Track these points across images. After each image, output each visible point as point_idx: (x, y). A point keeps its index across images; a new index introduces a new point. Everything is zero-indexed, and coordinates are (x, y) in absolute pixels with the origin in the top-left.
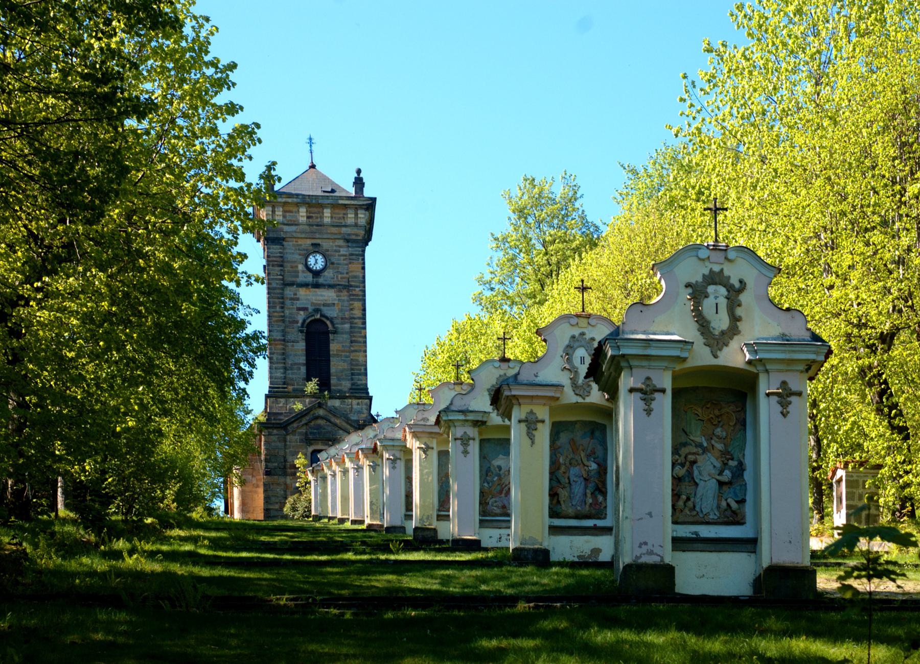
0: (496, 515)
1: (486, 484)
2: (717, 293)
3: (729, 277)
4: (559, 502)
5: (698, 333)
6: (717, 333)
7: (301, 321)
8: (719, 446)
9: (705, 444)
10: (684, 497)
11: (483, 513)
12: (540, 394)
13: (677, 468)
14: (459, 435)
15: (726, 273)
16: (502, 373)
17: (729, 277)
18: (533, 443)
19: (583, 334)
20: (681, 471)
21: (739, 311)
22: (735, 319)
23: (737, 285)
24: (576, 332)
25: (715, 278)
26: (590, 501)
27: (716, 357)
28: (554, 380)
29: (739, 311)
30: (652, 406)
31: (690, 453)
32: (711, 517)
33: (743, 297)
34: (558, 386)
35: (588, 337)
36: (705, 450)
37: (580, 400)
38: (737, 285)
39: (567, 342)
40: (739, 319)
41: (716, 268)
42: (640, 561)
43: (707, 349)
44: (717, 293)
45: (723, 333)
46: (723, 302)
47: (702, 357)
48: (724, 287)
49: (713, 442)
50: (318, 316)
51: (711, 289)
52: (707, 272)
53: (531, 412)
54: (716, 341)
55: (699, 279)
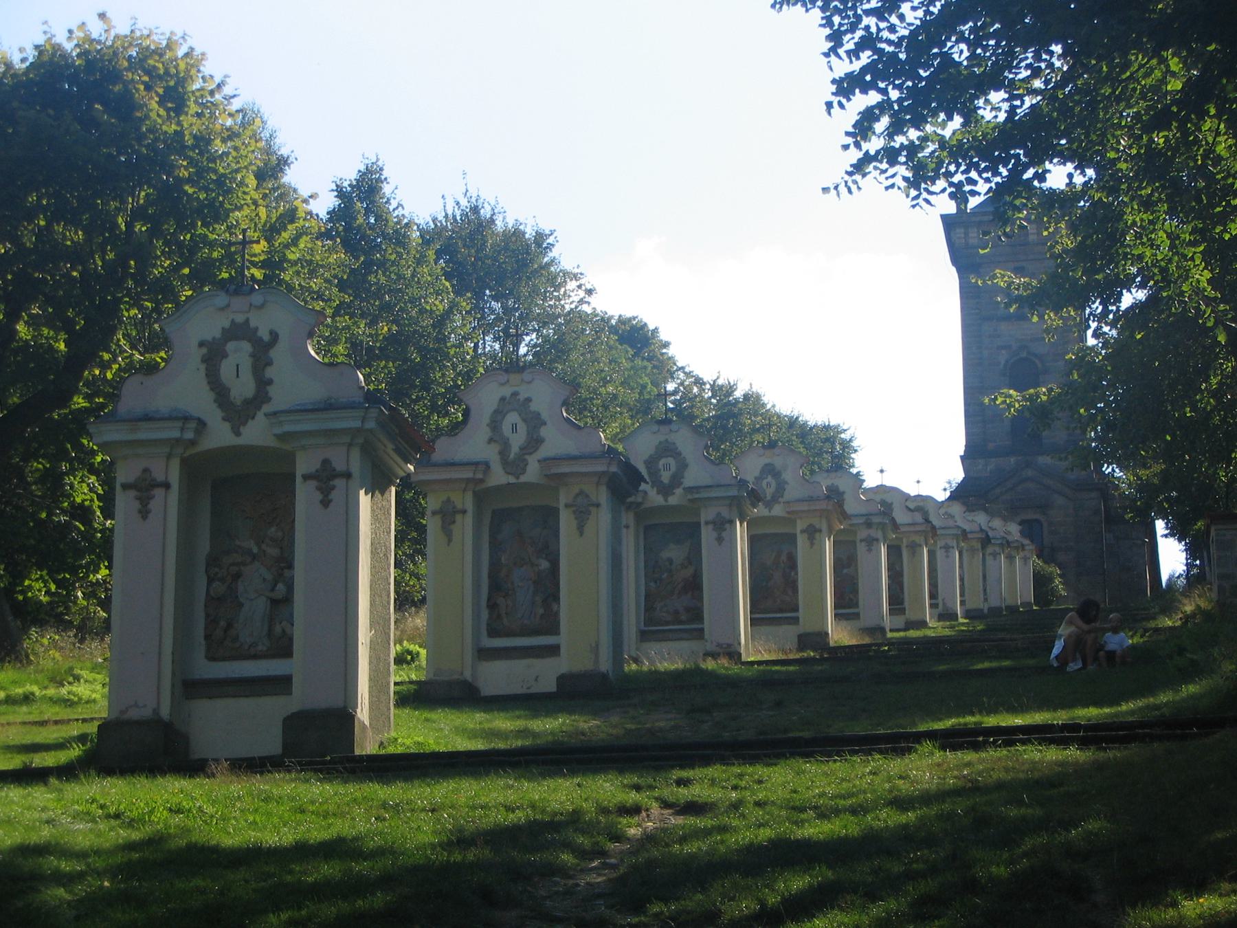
0: (667, 623)
1: (652, 584)
2: (239, 355)
3: (257, 329)
4: (499, 616)
5: (214, 406)
6: (239, 403)
7: (1003, 362)
8: (273, 551)
9: (255, 550)
10: (223, 623)
11: (649, 621)
12: (584, 470)
13: (216, 584)
14: (710, 518)
15: (253, 324)
16: (662, 438)
17: (257, 329)
18: (450, 541)
19: (515, 394)
20: (219, 588)
21: (270, 372)
22: (263, 384)
23: (266, 338)
24: (507, 391)
25: (238, 331)
26: (541, 611)
27: (238, 434)
28: (479, 457)
29: (270, 372)
30: (150, 506)
31: (233, 564)
32: (260, 648)
33: (273, 353)
34: (487, 465)
35: (521, 397)
36: (254, 557)
37: (512, 480)
38: (266, 338)
39: (495, 406)
40: (270, 382)
41: (240, 318)
42: (126, 717)
43: (227, 425)
44: (239, 355)
45: (247, 402)
46: (246, 364)
47: (220, 435)
48: (249, 341)
49: (264, 546)
50: (1024, 355)
51: (230, 346)
52: (227, 324)
53: (448, 500)
54: (238, 414)
55: (218, 335)
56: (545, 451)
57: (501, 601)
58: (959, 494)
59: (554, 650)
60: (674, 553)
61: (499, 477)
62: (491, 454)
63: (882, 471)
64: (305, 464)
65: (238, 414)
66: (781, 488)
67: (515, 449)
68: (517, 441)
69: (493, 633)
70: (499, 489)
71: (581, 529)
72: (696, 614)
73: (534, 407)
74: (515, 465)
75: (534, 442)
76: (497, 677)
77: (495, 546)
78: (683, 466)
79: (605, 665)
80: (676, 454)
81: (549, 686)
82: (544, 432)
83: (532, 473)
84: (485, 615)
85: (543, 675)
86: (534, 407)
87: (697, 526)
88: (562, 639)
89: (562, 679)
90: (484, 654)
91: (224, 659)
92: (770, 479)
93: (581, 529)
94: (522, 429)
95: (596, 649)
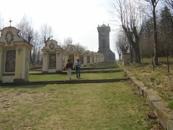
34: (4, 43)
54: (52, 49)
56: (14, 41)
57: (7, 66)
58: (98, 52)
59: (14, 75)
60: (53, 57)
61: (6, 45)
62: (5, 41)
63: (11, 21)
64: (57, 53)
65: (52, 49)
66: (73, 50)
67: (9, 40)
68: (9, 39)
69: (6, 71)
70: (6, 47)
71: (19, 54)
72: (55, 66)
73: (13, 33)
74: (9, 43)
75: (12, 39)
76: (50, 71)
77: (7, 56)
78: (54, 46)
79: (23, 77)
80: (53, 44)
81: (12, 81)
82: (14, 37)
83: (12, 45)
84: (5, 68)
85: (54, 71)
86: (13, 33)
87: (15, 51)
88: (16, 72)
89: (15, 80)
90: (4, 75)
91: (15, 68)
92: (9, 35)
93: (19, 54)
94: (10, 37)
95: (21, 75)
